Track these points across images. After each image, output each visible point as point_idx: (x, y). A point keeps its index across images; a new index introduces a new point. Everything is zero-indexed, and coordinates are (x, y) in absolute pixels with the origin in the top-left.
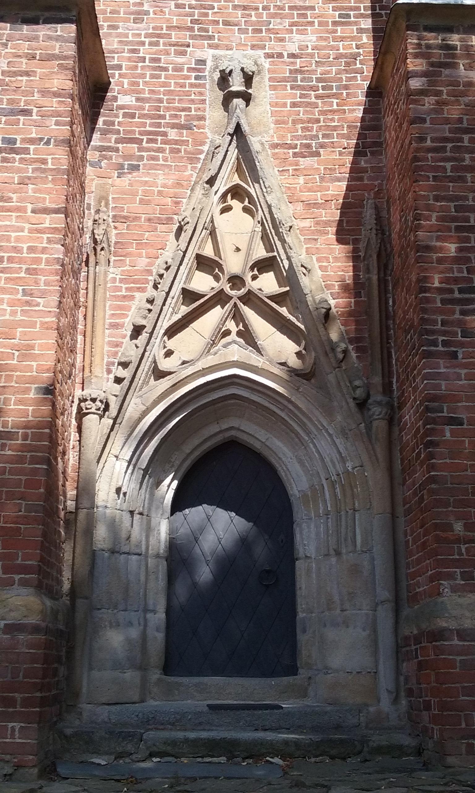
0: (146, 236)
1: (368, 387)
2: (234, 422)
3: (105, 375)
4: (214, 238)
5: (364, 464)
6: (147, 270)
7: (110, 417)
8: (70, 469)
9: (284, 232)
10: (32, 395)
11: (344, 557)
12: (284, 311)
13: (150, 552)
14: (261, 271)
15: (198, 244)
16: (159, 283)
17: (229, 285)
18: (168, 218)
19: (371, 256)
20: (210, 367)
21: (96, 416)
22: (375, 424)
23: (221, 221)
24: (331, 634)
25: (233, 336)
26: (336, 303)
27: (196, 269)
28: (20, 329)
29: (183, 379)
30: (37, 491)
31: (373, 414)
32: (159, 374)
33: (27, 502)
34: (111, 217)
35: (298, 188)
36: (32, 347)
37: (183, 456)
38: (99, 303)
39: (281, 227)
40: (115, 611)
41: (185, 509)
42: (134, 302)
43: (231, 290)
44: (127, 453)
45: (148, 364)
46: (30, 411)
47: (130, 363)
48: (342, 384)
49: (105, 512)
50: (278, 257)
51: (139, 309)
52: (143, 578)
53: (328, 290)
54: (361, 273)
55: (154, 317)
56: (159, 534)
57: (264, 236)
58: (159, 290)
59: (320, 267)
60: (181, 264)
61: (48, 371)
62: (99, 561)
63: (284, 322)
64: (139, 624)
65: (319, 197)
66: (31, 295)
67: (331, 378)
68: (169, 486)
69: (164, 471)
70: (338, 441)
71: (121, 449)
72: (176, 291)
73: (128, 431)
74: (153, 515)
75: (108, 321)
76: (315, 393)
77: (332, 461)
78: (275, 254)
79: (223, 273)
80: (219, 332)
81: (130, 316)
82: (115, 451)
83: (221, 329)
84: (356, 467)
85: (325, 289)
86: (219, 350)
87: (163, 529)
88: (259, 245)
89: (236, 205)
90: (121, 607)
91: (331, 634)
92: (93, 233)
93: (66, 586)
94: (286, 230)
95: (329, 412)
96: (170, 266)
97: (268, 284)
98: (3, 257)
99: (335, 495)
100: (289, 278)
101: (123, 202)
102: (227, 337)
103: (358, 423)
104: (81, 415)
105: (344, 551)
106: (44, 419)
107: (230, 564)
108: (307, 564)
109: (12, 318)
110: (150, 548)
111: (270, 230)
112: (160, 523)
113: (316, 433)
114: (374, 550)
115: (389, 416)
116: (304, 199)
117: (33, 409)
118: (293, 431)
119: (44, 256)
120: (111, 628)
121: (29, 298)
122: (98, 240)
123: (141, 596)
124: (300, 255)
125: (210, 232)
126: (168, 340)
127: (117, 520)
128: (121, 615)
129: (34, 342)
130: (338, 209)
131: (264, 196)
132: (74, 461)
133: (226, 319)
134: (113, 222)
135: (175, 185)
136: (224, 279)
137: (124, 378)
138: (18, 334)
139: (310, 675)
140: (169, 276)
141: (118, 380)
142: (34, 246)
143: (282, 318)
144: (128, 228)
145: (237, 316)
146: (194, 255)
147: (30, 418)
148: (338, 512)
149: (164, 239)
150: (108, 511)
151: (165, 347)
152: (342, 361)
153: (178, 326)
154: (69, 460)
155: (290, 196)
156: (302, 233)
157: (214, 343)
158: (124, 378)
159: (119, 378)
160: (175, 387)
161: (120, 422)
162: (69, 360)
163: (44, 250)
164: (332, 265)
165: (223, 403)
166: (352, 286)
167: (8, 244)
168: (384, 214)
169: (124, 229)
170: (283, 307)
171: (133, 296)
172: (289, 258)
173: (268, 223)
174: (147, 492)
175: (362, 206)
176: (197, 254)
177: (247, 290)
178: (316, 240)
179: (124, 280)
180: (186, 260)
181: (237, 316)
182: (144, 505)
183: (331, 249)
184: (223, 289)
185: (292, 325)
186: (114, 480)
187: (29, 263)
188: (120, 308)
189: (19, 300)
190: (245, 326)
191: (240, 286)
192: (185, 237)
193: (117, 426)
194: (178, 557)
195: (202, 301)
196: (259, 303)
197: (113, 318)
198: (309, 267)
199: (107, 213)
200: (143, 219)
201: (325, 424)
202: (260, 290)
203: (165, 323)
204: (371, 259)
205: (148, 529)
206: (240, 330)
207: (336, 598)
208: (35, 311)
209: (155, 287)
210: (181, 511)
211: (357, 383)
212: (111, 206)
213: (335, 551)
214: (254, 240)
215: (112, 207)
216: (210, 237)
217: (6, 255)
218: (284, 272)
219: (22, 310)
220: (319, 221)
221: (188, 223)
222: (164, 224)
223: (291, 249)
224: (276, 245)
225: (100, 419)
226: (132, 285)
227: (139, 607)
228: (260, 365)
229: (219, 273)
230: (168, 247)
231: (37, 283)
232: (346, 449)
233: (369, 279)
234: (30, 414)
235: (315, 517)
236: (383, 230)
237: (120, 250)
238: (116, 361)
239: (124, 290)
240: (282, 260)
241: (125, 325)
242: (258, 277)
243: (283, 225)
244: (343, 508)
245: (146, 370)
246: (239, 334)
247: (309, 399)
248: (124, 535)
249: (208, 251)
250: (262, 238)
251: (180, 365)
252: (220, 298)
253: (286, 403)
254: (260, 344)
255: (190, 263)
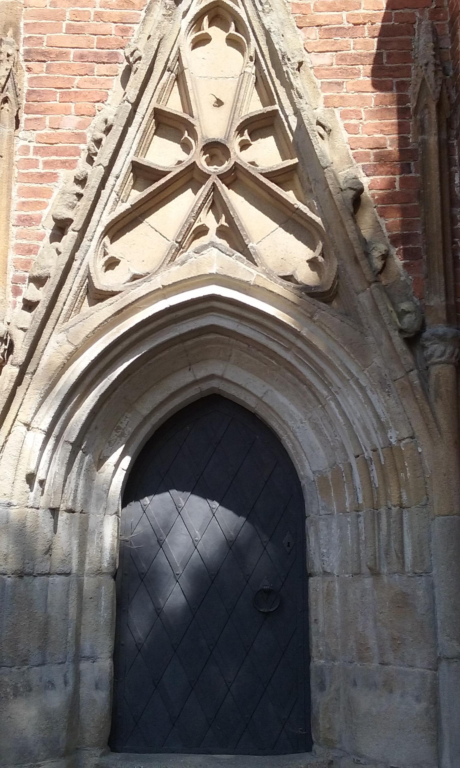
0: (76, 82)
1: (422, 311)
2: (216, 368)
3: (11, 298)
4: (182, 86)
5: (417, 434)
7: (15, 362)
9: (290, 71)
11: (385, 579)
12: (290, 196)
13: (87, 567)
17: (205, 157)
18: (109, 54)
19: (426, 106)
20: (174, 284)
22: (434, 370)
23: (195, 61)
24: (366, 701)
26: (371, 183)
27: (154, 134)
29: (133, 302)
31: (431, 356)
32: (96, 296)
34: (21, 51)
35: (312, 6)
37: (139, 419)
39: (286, 64)
41: (143, 498)
42: (57, 184)
45: (78, 279)
47: (47, 277)
48: (381, 307)
49: (8, 513)
50: (280, 112)
52: (73, 611)
53: (358, 162)
54: (410, 135)
55: (85, 206)
57: (260, 80)
59: (347, 127)
63: (289, 213)
64: (66, 683)
65: (345, 18)
67: (364, 299)
68: (117, 466)
69: (109, 442)
70: (374, 398)
71: (35, 414)
72: (122, 165)
73: (45, 385)
74: (92, 509)
76: (338, 321)
77: (365, 428)
78: (277, 107)
81: (50, 206)
82: (24, 416)
83: (191, 225)
84: (404, 439)
85: (354, 161)
86: (189, 257)
89: (218, 35)
90: (35, 658)
91: (366, 701)
94: (293, 69)
95: (360, 351)
96: (111, 126)
97: (265, 155)
99: (371, 482)
100: (299, 145)
101: (42, 30)
102: (202, 238)
103: (408, 370)
105: (384, 570)
107: (211, 581)
108: (326, 584)
110: (87, 561)
111: (268, 71)
112: (102, 521)
113: (340, 384)
114: (434, 572)
115: (456, 358)
116: (321, 22)
118: (303, 381)
120: (15, 695)
123: (69, 639)
124: (314, 108)
125: (177, 76)
126: (111, 243)
127: (28, 524)
128: (35, 675)
130: (374, 37)
131: (259, 18)
133: (200, 209)
134: (26, 61)
135: (121, 4)
136: (197, 147)
137: (38, 302)
139: (330, 758)
140: (109, 143)
141: (29, 306)
143: (287, 207)
144: (48, 70)
145: (217, 205)
146: (150, 111)
148: (375, 507)
151: (105, 254)
152: (380, 272)
153: (127, 220)
155: (299, 17)
156: (318, 74)
157: (181, 247)
158: (38, 302)
159: (30, 301)
160: (120, 314)
161: (32, 370)
164: (365, 123)
166: (396, 155)
168: (446, 44)
169: (42, 72)
170: (288, 190)
171: (55, 174)
172: (297, 113)
174: (82, 478)
175: (412, 32)
177: (233, 163)
178: (339, 84)
180: (138, 118)
181: (217, 205)
183: (362, 98)
184: (194, 162)
185: (302, 218)
186: (23, 461)
188: (35, 193)
190: (230, 219)
191: (221, 157)
192: (136, 80)
193: (27, 377)
194: (133, 570)
195: (163, 181)
196: (251, 184)
197: (25, 209)
198: (329, 125)
199: (16, 46)
200: (71, 56)
201: (354, 370)
202: (253, 163)
203: (104, 216)
204: (426, 111)
205: (84, 535)
206: (222, 226)
207: (372, 642)
209: (90, 160)
211: (405, 306)
212: (22, 37)
213: (370, 569)
214: (244, 86)
215: (25, 38)
218: (290, 135)
220: (344, 55)
221: (140, 58)
222: (104, 63)
223: (301, 98)
227: (66, 657)
228: (252, 280)
230: (110, 99)
232: (388, 410)
233: (424, 143)
235: (339, 512)
236: (444, 68)
237: (36, 104)
239: (41, 165)
240: (286, 117)
241: (43, 220)
242: (251, 145)
243: (289, 60)
244: (382, 502)
245: (75, 289)
246: (221, 232)
247: (329, 332)
248: (40, 547)
249: (174, 105)
251: (128, 282)
252: (191, 177)
253: (292, 338)
254: (252, 247)
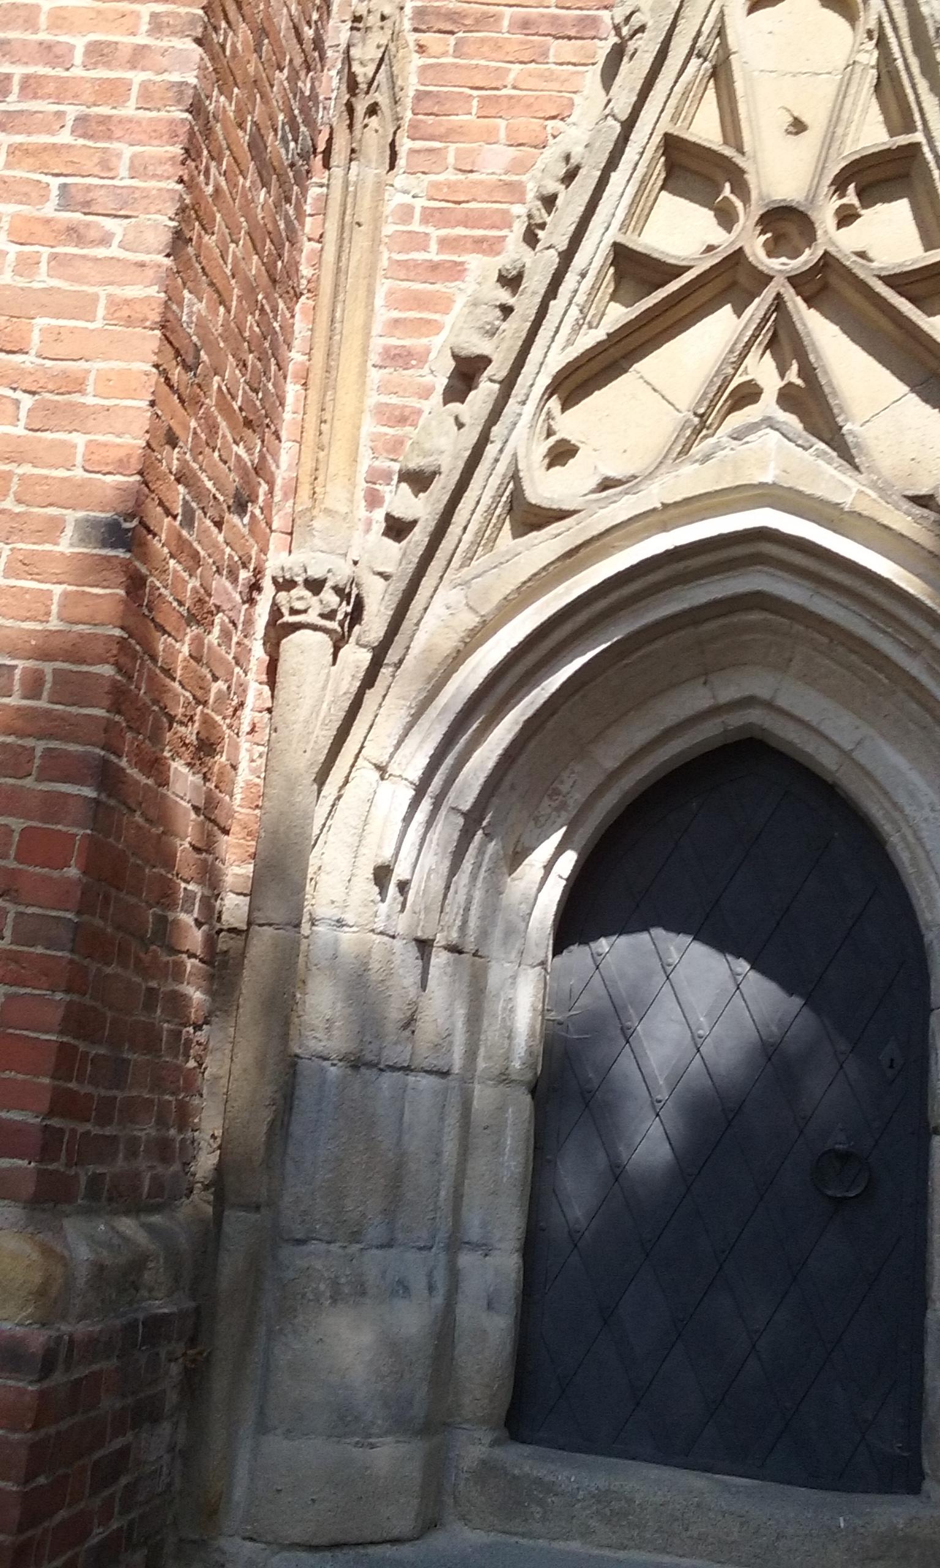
0: (512, 76)
3: (361, 511)
4: (724, 92)
6: (507, 184)
7: (363, 641)
8: (238, 797)
10: (66, 545)
13: (481, 1064)
14: (870, 195)
15: (673, 102)
16: (542, 226)
17: (763, 238)
18: (582, 20)
20: (687, 501)
21: (320, 635)
25: (768, 404)
27: (662, 188)
28: (41, 322)
30: (56, 874)
32: (530, 518)
33: (21, 909)
34: (408, 11)
36: (78, 385)
37: (595, 780)
38: (353, 283)
40: (356, 1247)
41: (595, 938)
42: (462, 286)
43: (770, 254)
44: (414, 760)
45: (495, 482)
46: (56, 599)
49: (336, 940)
50: (926, 149)
51: (475, 304)
52: (450, 1148)
55: (517, 331)
56: (512, 1010)
58: (539, 247)
60: (612, 163)
61: (120, 467)
62: (306, 1092)
64: (431, 1288)
66: (87, 207)
68: (548, 868)
69: (536, 819)
71: (397, 747)
72: (594, 251)
73: (420, 691)
75: (378, 344)
78: (919, 137)
79: (745, 198)
80: (721, 389)
82: (376, 751)
83: (727, 380)
87: (522, 1003)
88: (865, 111)
90: (375, 1232)
92: (348, 59)
93: (206, 1162)
96: (578, 168)
98: (8, 77)
104: (279, 630)
106: (99, 630)
107: (724, 1120)
109: (21, 282)
110: (482, 1052)
111: (905, 60)
112: (514, 977)
117: (65, 595)
119: (137, 77)
120: (334, 1300)
121: (78, 216)
122: (360, 79)
123: (441, 1203)
125: (714, 67)
126: (563, 410)
127: (374, 966)
128: (373, 1263)
129: (82, 364)
132: (253, 771)
133: (748, 346)
134: (416, 30)
136: (747, 217)
137: (414, 523)
138: (36, 337)
141: (397, 529)
142: (109, 44)
144: (458, 52)
145: (783, 340)
146: (657, 139)
147: (54, 624)
149: (567, 86)
150: (346, 937)
151: (550, 433)
153: (595, 366)
154: (234, 767)
158: (414, 523)
160: (574, 558)
161: (396, 660)
162: (240, 450)
163: (138, 57)
165: (722, 621)
167: (29, 36)
169: (444, 54)
171: (462, 263)
173: (898, 37)
174: (479, 884)
176: (666, 135)
177: (820, 253)
179: (437, 215)
181: (783, 340)
182: (465, 922)
186: (371, 840)
187: (87, 97)
188: (419, 301)
189: (48, 221)
190: (808, 372)
191: (797, 240)
192: (631, 73)
193: (386, 672)
194: (568, 1080)
197: (397, 333)
200: (506, 23)
202: (862, 255)
203: (553, 355)
205: (477, 996)
206: (790, 384)
208: (96, 260)
209: (531, 239)
210: (586, 943)
214: (852, 91)
216: (712, 83)
217: (18, 71)
219: (54, 257)
221: (642, 29)
222: (570, 38)
224: (921, 110)
225: (337, 649)
226: (461, 231)
228: (847, 500)
229: (733, 198)
231: (106, 166)
234: (54, 608)
238: (396, 467)
239: (434, 246)
241: (432, 356)
242: (859, 216)
245: (486, 500)
248: (395, 1013)
249: (705, 128)
250: (878, 87)
251: (593, 492)
252: (731, 280)
254: (851, 432)
255: (644, 163)
